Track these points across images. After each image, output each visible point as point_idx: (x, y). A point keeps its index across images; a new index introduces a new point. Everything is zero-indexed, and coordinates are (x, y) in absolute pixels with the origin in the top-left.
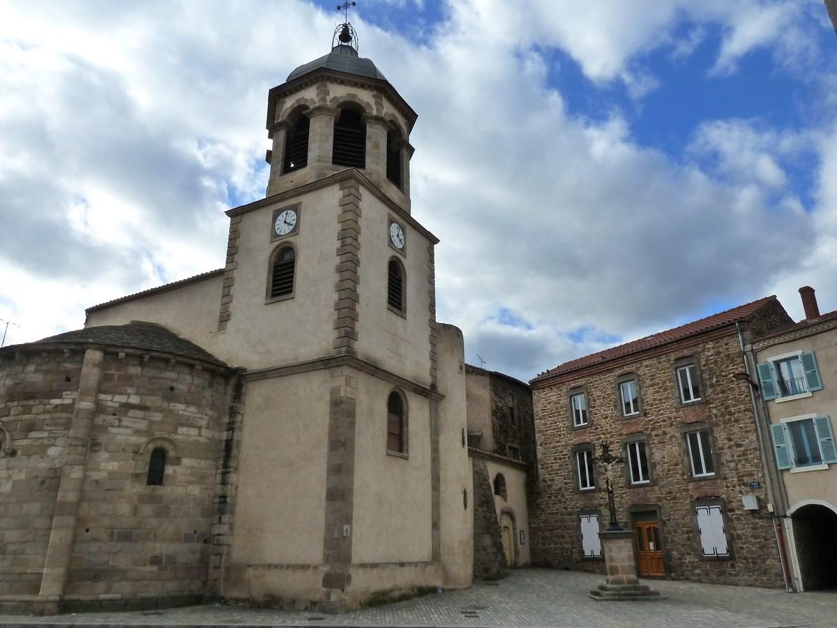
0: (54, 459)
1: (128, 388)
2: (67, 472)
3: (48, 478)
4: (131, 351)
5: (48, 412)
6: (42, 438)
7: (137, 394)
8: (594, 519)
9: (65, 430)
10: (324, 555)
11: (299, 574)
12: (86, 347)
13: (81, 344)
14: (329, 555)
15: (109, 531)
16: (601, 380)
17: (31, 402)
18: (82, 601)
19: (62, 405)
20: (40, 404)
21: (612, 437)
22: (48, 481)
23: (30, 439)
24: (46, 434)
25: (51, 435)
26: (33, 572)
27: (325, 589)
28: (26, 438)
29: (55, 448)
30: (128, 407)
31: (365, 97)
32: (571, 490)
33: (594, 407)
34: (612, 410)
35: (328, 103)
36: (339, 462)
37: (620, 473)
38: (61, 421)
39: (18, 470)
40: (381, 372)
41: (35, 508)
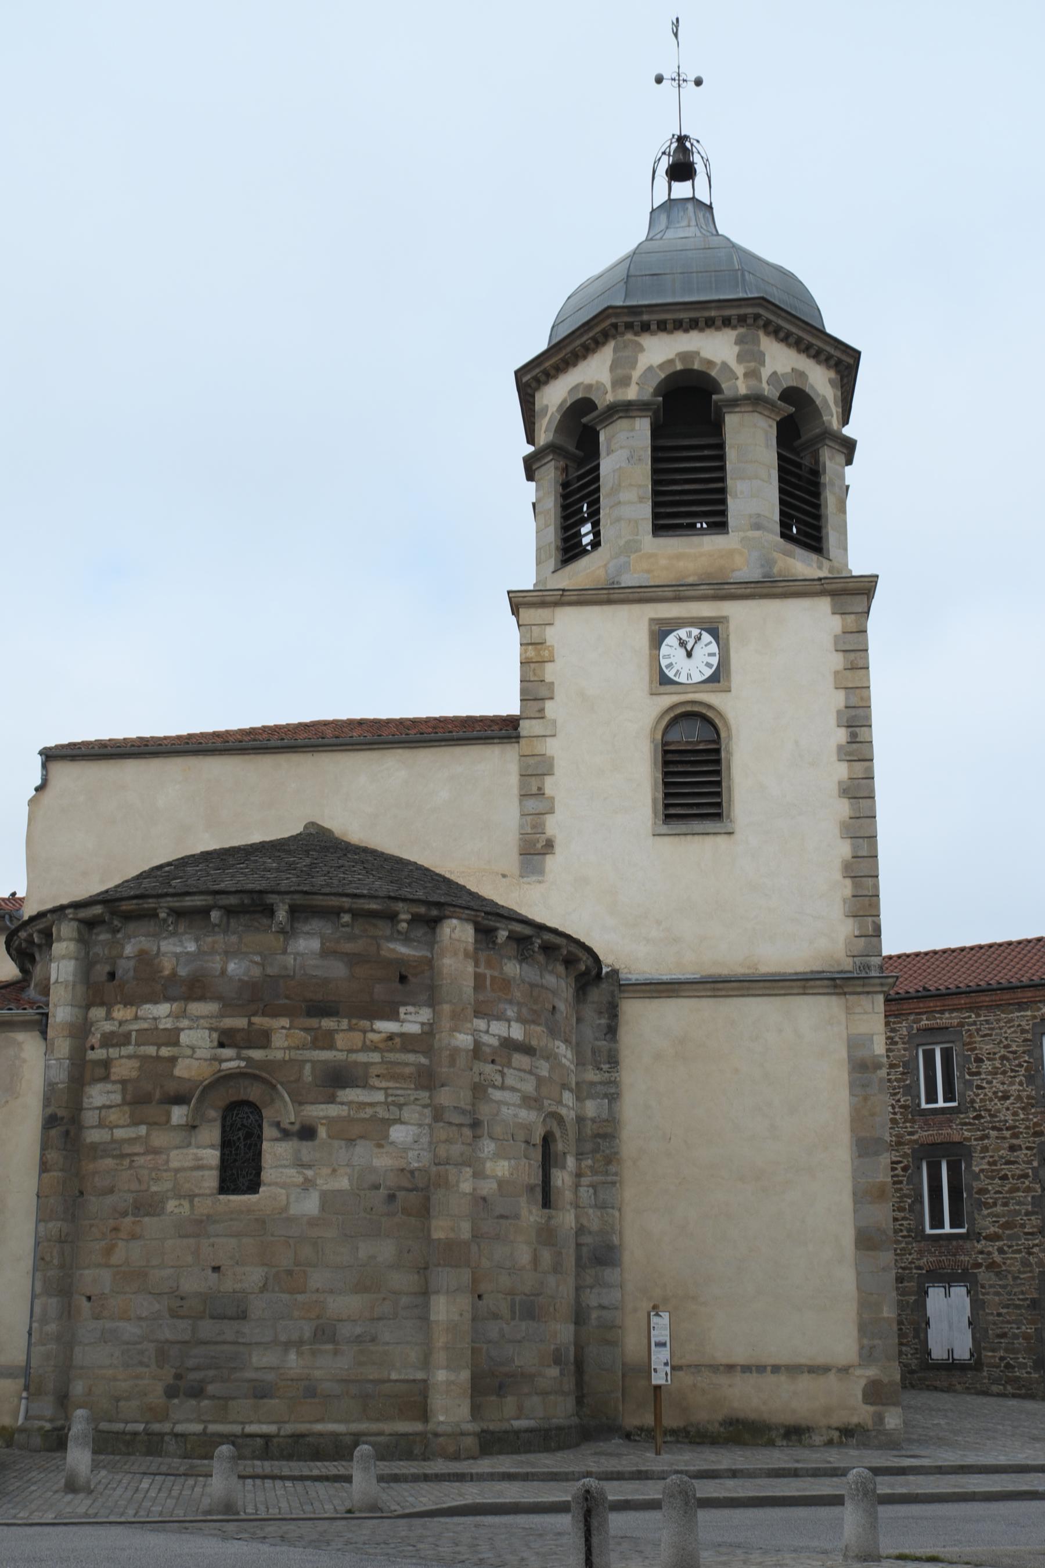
0: (405, 1150)
1: (507, 1006)
2: (452, 1179)
3: (401, 1188)
4: (422, 910)
5: (375, 1049)
6: (372, 1105)
7: (520, 1020)
8: (959, 1292)
9: (416, 1089)
10: (862, 1348)
11: (805, 1382)
12: (447, 913)
13: (439, 905)
14: (872, 1347)
15: (509, 1298)
16: (998, 1021)
17: (328, 1023)
18: (492, 1433)
19: (402, 1035)
20: (351, 1029)
21: (1015, 1136)
22: (401, 1195)
23: (342, 1104)
24: (380, 1097)
25: (390, 1099)
26: (402, 1377)
27: (871, 1409)
28: (332, 1100)
29: (402, 1127)
30: (509, 1045)
31: (717, 349)
32: (905, 1233)
33: (978, 1073)
34: (1021, 1084)
35: (765, 385)
36: (881, 1179)
37: (1030, 1208)
38: (407, 1070)
39: (329, 1171)
40: (687, 987)
41: (385, 1250)
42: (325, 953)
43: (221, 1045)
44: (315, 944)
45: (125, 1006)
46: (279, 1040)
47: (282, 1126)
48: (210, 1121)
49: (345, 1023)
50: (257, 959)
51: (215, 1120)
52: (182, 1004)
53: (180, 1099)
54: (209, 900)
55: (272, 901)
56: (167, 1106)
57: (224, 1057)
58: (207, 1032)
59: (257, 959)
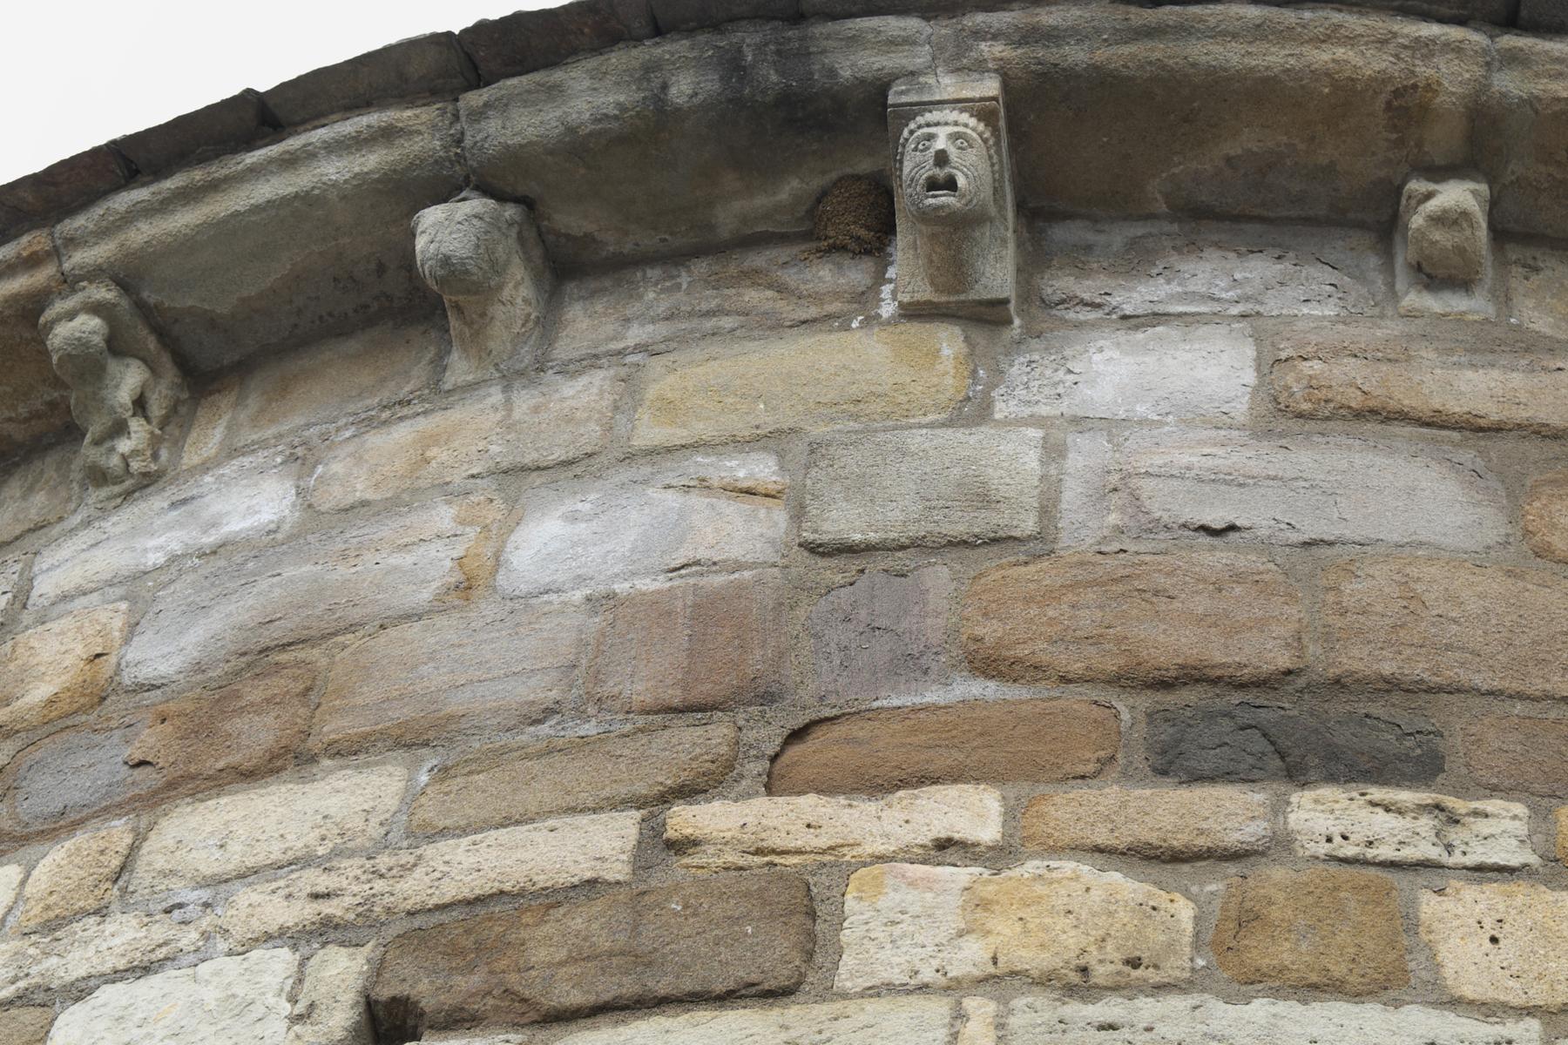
42: (1289, 413)
44: (1218, 369)
45: (418, 1002)
49: (1502, 831)
50: (761, 469)
54: (420, 130)
59: (761, 469)
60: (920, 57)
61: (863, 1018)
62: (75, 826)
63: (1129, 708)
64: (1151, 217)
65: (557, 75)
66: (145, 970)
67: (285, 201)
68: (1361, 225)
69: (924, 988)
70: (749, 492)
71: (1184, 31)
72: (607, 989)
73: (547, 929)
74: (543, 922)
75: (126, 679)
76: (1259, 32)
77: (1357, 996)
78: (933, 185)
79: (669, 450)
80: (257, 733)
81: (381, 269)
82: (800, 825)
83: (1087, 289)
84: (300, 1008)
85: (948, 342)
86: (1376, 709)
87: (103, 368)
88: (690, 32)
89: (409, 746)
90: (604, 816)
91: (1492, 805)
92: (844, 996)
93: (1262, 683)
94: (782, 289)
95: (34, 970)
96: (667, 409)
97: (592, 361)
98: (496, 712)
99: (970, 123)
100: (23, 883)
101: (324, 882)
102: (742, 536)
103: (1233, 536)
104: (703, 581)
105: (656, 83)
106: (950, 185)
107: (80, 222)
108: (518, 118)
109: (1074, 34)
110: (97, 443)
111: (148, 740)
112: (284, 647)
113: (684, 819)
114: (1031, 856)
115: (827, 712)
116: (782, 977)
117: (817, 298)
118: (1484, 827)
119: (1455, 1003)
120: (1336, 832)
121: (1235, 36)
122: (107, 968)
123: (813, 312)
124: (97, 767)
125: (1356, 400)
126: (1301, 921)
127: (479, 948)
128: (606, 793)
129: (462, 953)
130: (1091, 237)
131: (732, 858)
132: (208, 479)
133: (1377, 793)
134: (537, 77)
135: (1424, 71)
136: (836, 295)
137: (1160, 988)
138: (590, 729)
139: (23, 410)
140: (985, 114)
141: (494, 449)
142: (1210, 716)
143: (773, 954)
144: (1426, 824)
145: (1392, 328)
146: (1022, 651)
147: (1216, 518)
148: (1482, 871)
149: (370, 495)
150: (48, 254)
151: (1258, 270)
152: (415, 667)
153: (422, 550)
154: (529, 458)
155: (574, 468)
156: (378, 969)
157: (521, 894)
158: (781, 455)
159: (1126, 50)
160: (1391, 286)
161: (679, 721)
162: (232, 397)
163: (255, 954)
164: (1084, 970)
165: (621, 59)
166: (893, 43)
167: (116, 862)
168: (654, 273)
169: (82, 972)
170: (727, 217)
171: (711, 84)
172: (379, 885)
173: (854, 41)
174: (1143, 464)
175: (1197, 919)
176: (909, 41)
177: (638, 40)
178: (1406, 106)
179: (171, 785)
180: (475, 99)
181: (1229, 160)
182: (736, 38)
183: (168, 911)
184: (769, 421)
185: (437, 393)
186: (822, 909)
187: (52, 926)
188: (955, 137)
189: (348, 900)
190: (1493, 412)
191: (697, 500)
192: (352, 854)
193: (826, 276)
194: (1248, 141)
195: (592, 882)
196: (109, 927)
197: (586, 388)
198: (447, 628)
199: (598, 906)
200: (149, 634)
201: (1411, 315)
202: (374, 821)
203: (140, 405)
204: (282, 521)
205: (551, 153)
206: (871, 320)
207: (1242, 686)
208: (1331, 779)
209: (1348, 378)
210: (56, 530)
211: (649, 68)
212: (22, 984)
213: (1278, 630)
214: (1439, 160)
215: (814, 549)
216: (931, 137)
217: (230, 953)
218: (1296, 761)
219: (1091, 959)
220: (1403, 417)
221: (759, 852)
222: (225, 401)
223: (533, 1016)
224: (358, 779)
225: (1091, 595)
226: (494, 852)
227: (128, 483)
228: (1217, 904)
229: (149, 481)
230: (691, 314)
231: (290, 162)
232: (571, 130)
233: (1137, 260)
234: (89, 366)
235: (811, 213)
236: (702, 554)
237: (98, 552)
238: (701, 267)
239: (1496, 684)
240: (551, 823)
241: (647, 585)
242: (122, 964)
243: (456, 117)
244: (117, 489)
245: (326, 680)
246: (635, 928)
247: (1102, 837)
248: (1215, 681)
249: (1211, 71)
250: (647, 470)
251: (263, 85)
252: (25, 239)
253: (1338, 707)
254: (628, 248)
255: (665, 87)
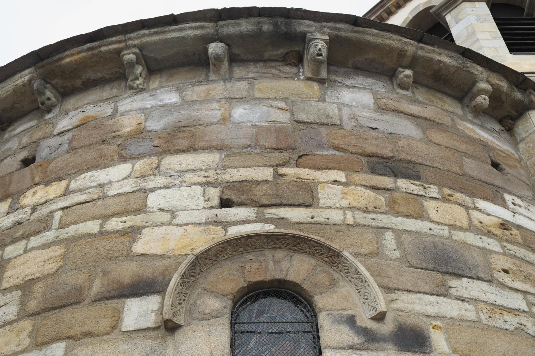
28: (443, 292)
43: (225, 203)
46: (329, 195)
47: (359, 323)
48: (207, 317)
50: (282, 105)
51: (217, 315)
52: (155, 160)
53: (140, 288)
54: (209, 28)
55: (303, 29)
56: (114, 303)
57: (232, 219)
58: (199, 190)
60: (313, 29)
61: (326, 212)
62: (143, 157)
63: (364, 160)
64: (348, 67)
65: (239, 21)
66: (168, 187)
67: (179, 38)
68: (386, 75)
69: (337, 208)
70: (281, 109)
71: (363, 32)
72: (274, 201)
73: (257, 189)
74: (257, 187)
75: (147, 129)
76: (377, 35)
77: (416, 218)
78: (318, 54)
79: (262, 98)
80: (184, 143)
81: (194, 54)
82: (306, 174)
83: (339, 79)
84: (206, 198)
85: (316, 86)
86: (408, 166)
87: (134, 66)
88: (266, 17)
89: (218, 150)
90: (265, 168)
91: (432, 186)
92: (322, 208)
93: (387, 158)
94: (279, 70)
95: (141, 185)
96: (260, 90)
97: (242, 79)
98: (237, 145)
99: (325, 44)
100: (133, 167)
101: (206, 174)
102: (283, 117)
103: (377, 130)
104: (276, 125)
105: (260, 26)
106: (321, 55)
107: (132, 35)
108: (230, 28)
109: (343, 30)
110: (131, 81)
111: (157, 142)
112: (185, 127)
113: (282, 170)
114: (352, 185)
115: (306, 153)
116: (309, 203)
117: (287, 73)
118: (430, 190)
119: (433, 222)
120: (407, 187)
121: (373, 35)
122: (159, 186)
123: (287, 76)
124: (145, 146)
125: (393, 108)
126: (404, 203)
127: (244, 190)
128: (265, 163)
129: (240, 191)
130: (337, 70)
131: (294, 179)
132: (158, 91)
133: (412, 182)
134: (235, 21)
135: (406, 48)
136: (291, 73)
137: (381, 213)
138: (258, 150)
139: (110, 72)
140: (326, 43)
141: (224, 93)
142: (379, 163)
143: (307, 199)
144: (421, 188)
145: (395, 96)
146: (343, 146)
147: (374, 126)
148: (432, 198)
149: (197, 99)
150: (124, 41)
151: (370, 81)
152: (217, 134)
153: (213, 111)
154: (232, 96)
155: (242, 100)
156: (222, 192)
157: (251, 181)
158: (286, 103)
159: (352, 34)
160: (393, 87)
161: (276, 151)
162: (159, 75)
163: (193, 187)
164: (366, 208)
165: (252, 20)
166: (308, 26)
167: (156, 165)
168: (252, 64)
169: (153, 186)
170: (266, 55)
171: (271, 28)
172: (219, 176)
173: (300, 24)
174: (358, 114)
175: (385, 201)
176: (311, 26)
177: (256, 17)
178: (401, 54)
179: (165, 151)
180: (221, 23)
181: (366, 59)
182: (277, 19)
183: (170, 176)
184: (283, 96)
185: (208, 81)
186: (314, 191)
187: (143, 176)
188: (322, 46)
189: (212, 179)
190: (417, 114)
191: (270, 109)
192: (211, 169)
193: (287, 69)
194: (370, 56)
195: (266, 180)
196: (157, 178)
197: (242, 84)
198: (222, 127)
199: (268, 185)
200: (151, 121)
201: (398, 93)
202: (214, 164)
203: (141, 75)
204: (177, 102)
205: (236, 36)
206: (299, 79)
207: (384, 158)
208: (403, 178)
209: (391, 103)
210: (121, 97)
211: (259, 23)
212: (139, 187)
213: (389, 149)
214: (404, 65)
215: (297, 121)
216: (317, 45)
217: (187, 186)
218: (396, 174)
219: (368, 206)
220: (401, 112)
221: (299, 178)
222: (158, 76)
223: (258, 205)
224: (209, 155)
225: (353, 137)
226: (243, 173)
227: (138, 90)
228: (388, 198)
229: (142, 90)
230: (262, 73)
231: (181, 30)
232: (241, 32)
233: (347, 75)
234: (132, 65)
235: (284, 57)
236: (275, 119)
237: (134, 103)
238: (261, 64)
239: (428, 164)
240: (254, 168)
241: (263, 124)
242: (162, 186)
243: (217, 26)
244: (135, 91)
245: (196, 135)
246: (277, 190)
247: (364, 183)
248: (379, 157)
249: (368, 41)
250: (258, 102)
251: (176, 13)
252: (119, 37)
253: (401, 165)
254: (246, 58)
255: (262, 27)
